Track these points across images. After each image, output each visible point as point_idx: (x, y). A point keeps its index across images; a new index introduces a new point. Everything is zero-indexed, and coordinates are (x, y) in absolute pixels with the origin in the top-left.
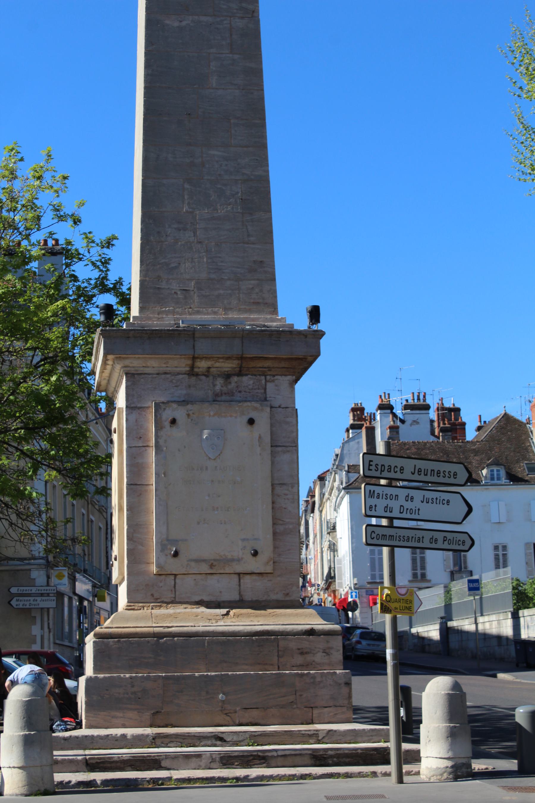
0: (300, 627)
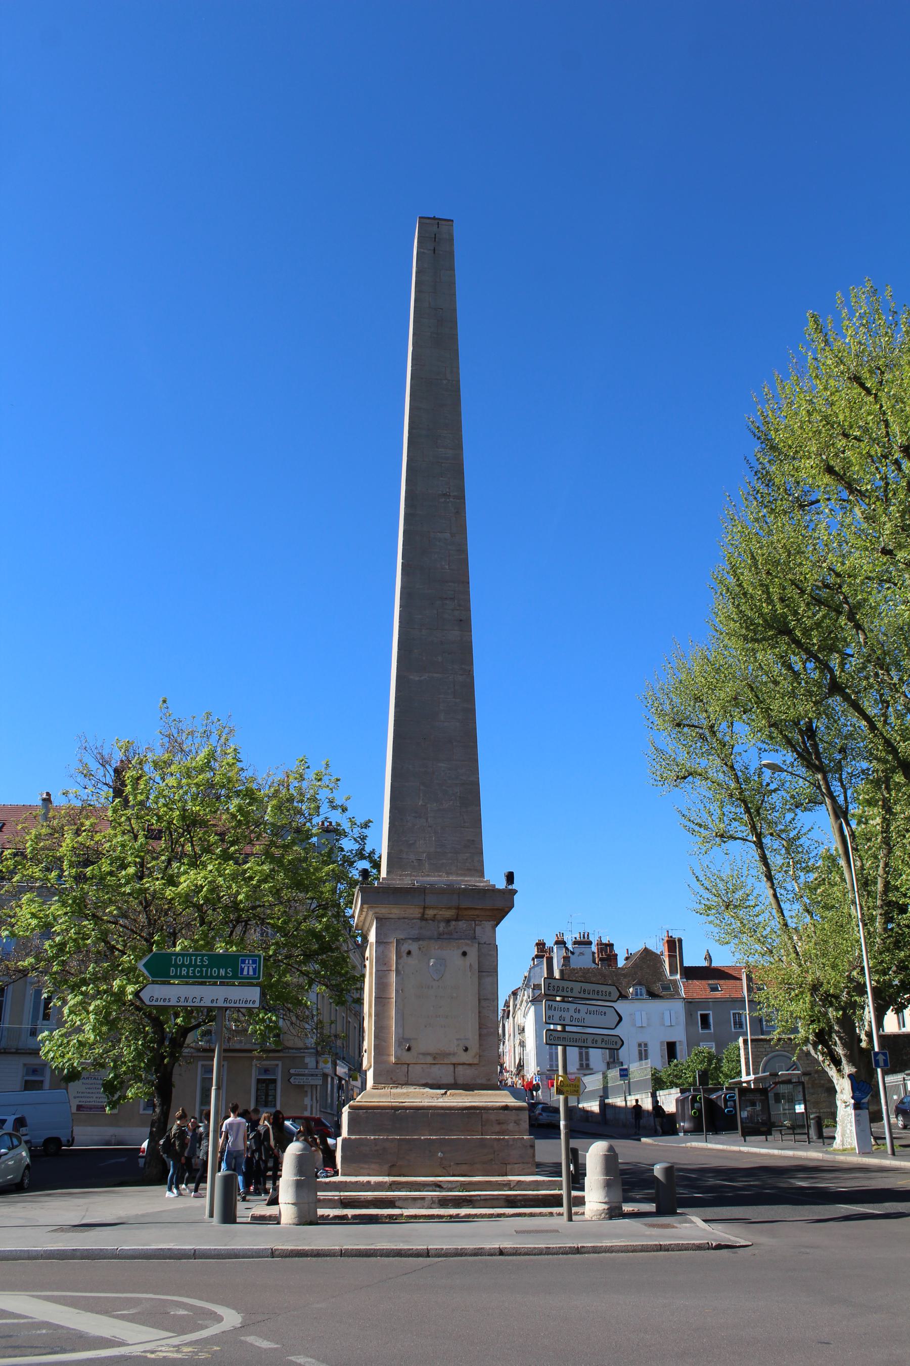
0: (498, 1104)
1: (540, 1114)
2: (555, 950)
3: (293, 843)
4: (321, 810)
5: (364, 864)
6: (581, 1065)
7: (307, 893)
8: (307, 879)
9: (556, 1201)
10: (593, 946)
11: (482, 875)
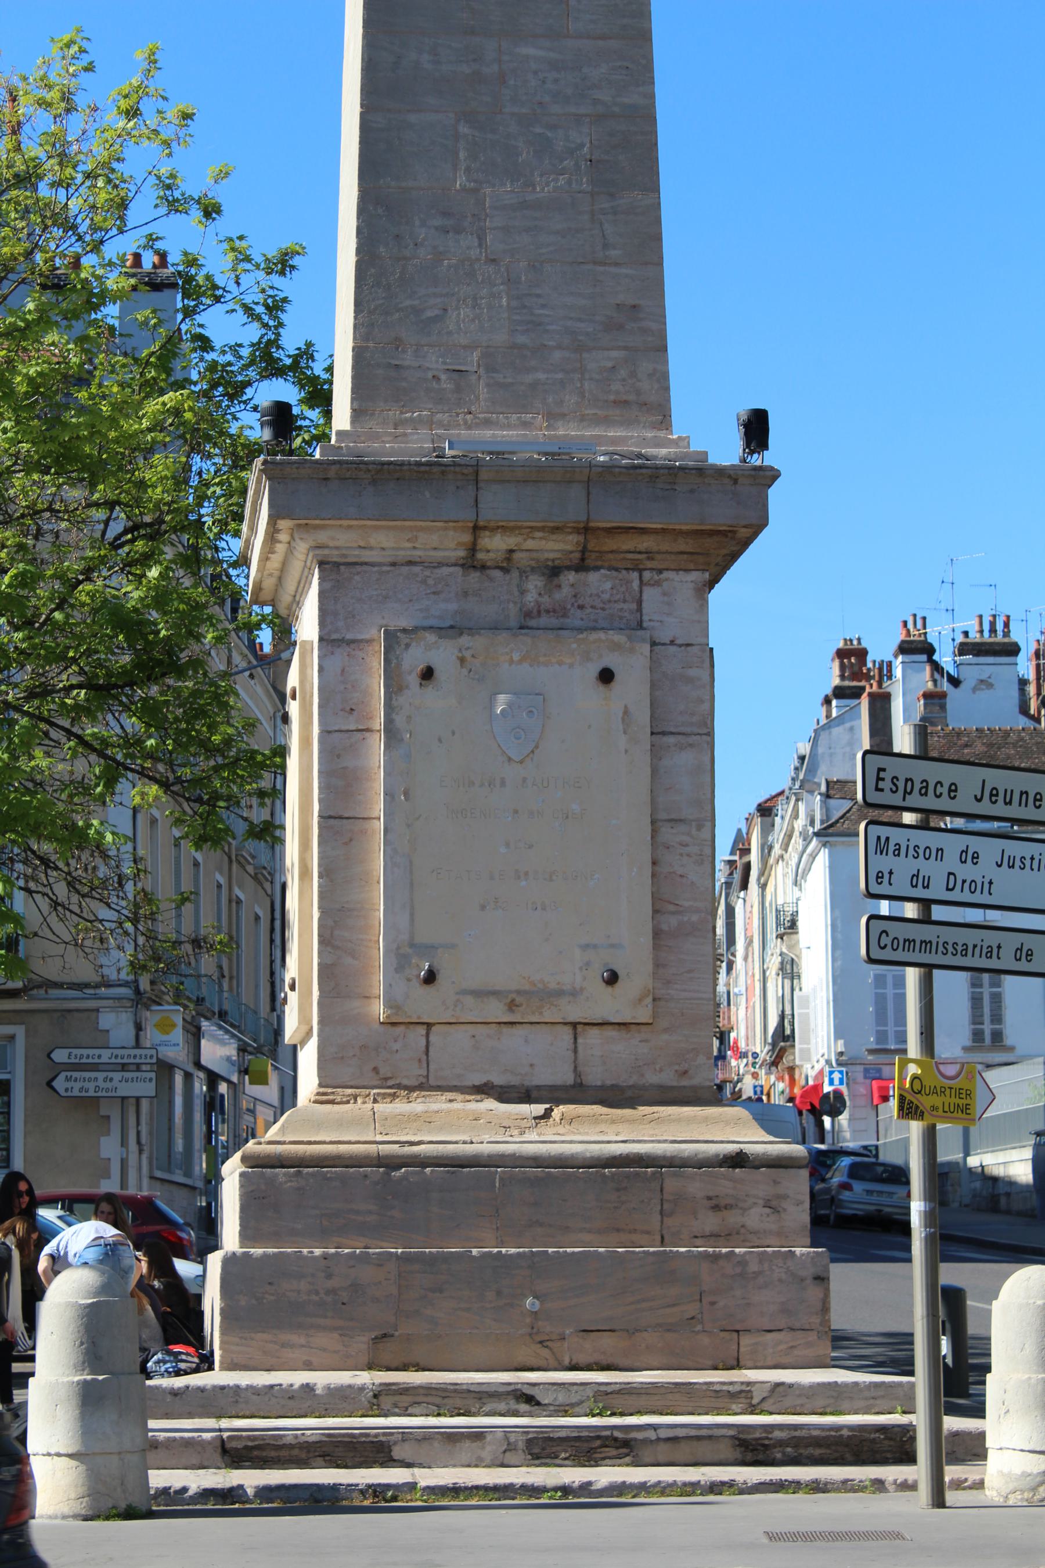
0: (713, 1149)
1: (845, 1186)
2: (898, 672)
3: (44, 320)
4: (135, 214)
5: (284, 390)
6: (977, 1036)
7: (93, 486)
8: (89, 439)
9: (896, 1447)
10: (1022, 655)
11: (664, 420)
